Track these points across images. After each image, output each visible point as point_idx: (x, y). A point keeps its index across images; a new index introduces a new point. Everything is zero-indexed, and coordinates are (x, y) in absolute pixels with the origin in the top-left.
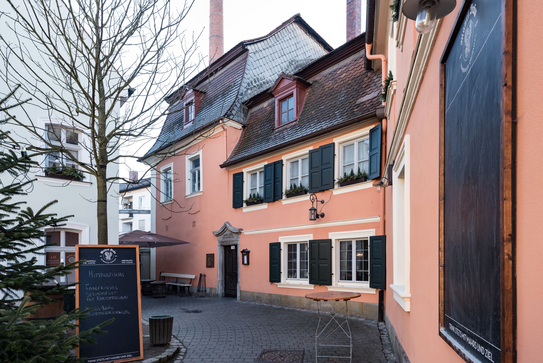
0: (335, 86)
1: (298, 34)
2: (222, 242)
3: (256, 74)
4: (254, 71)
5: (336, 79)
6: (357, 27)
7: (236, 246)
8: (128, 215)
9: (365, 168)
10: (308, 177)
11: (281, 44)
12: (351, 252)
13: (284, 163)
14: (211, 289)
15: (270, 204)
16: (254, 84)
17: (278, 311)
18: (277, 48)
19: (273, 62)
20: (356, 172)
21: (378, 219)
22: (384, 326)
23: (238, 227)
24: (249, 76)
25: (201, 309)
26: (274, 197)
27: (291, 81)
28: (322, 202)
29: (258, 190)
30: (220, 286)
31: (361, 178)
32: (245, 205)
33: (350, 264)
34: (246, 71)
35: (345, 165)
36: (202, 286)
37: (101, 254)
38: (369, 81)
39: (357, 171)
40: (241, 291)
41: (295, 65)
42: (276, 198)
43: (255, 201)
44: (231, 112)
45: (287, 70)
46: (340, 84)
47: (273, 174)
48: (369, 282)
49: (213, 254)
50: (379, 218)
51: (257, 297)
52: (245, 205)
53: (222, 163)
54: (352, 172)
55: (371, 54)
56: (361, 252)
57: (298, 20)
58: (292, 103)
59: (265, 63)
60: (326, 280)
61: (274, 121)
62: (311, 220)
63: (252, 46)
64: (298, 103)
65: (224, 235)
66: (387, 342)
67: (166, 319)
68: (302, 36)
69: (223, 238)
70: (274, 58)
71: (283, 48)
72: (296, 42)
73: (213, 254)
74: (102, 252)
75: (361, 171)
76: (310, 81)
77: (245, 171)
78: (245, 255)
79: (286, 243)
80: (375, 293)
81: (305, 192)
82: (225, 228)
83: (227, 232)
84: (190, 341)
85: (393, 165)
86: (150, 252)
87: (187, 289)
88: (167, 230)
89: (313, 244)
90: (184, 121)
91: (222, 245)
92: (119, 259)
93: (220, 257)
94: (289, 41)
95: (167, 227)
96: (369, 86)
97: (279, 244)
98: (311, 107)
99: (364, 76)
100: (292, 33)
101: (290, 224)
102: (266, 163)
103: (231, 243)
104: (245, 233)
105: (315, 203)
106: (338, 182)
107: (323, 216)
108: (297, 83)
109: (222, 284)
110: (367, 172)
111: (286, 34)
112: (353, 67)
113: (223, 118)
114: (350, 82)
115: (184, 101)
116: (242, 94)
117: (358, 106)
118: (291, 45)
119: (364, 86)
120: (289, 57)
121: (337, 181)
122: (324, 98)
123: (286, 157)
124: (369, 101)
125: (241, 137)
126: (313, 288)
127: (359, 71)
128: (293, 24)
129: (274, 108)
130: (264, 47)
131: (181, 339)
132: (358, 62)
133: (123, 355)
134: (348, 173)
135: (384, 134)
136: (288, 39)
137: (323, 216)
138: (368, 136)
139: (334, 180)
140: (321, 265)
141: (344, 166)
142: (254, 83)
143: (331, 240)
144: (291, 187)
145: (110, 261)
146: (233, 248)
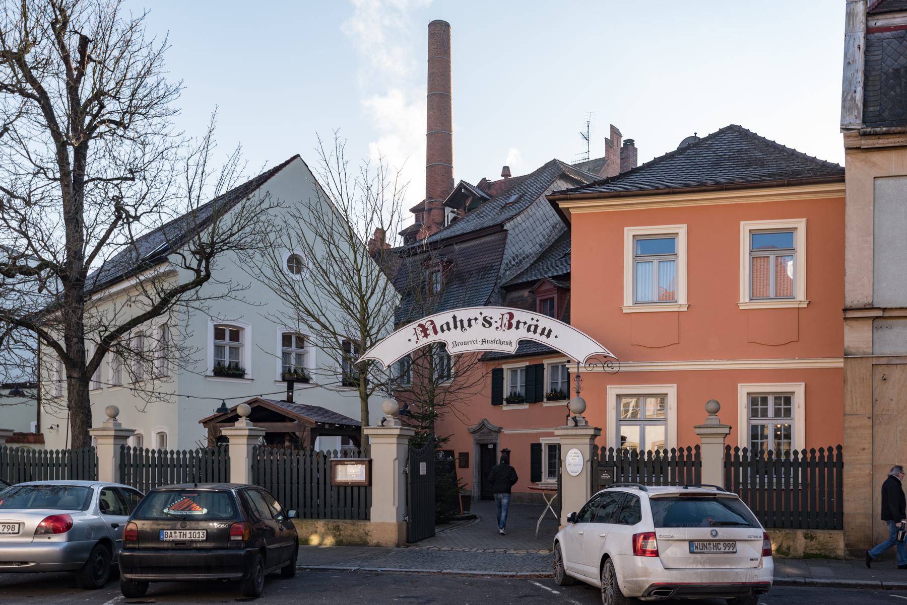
7: (495, 445)
13: (545, 366)
16: (513, 263)
23: (499, 426)
29: (519, 389)
32: (504, 402)
43: (514, 399)
52: (504, 402)
82: (483, 425)
83: (485, 430)
104: (506, 432)
146: (490, 446)
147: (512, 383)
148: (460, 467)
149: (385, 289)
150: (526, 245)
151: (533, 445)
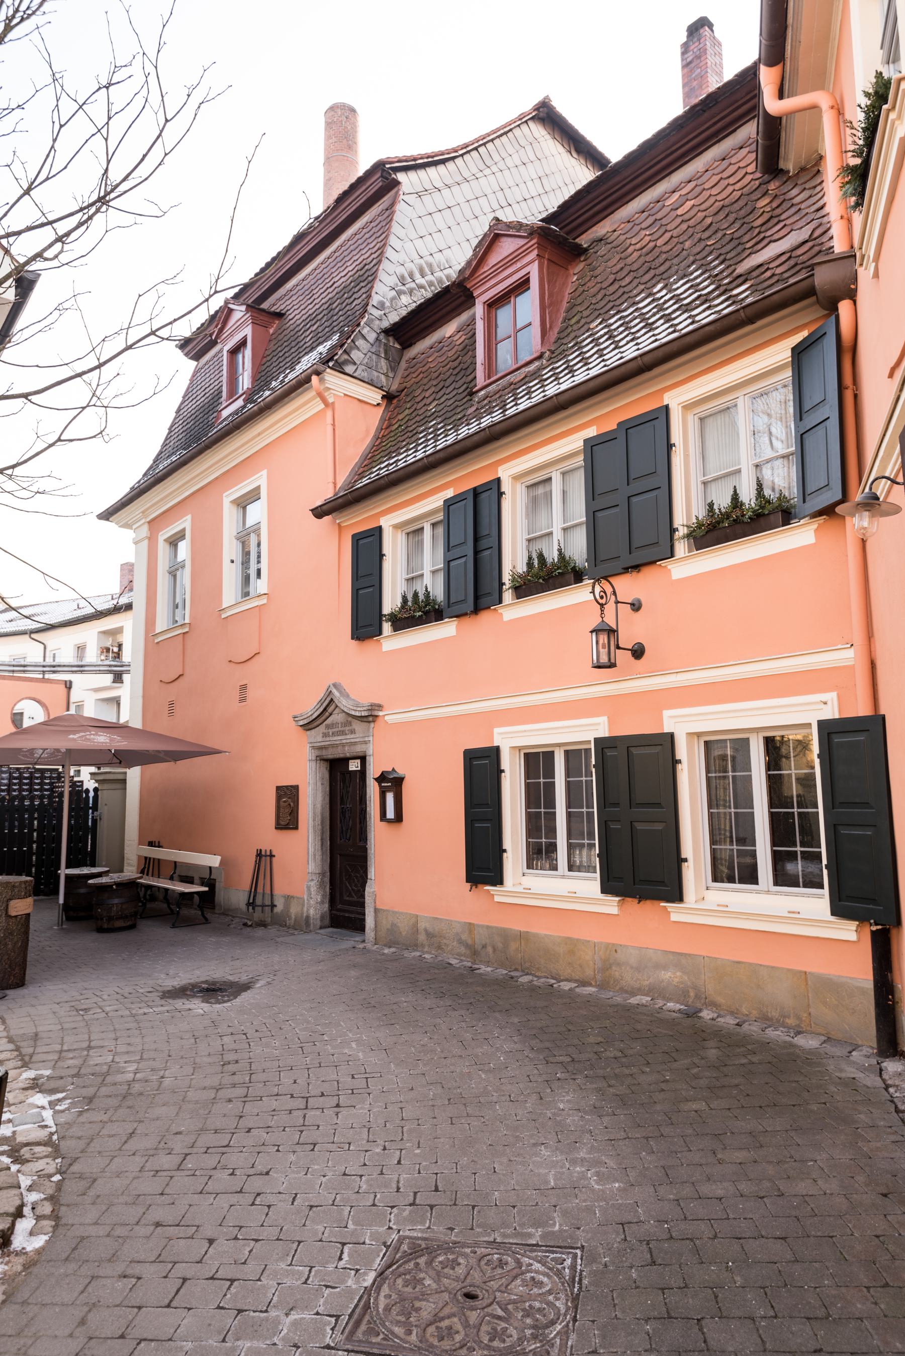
1: (547, 153)
2: (321, 748)
3: (424, 253)
4: (419, 243)
5: (664, 222)
7: (363, 759)
8: (110, 677)
10: (584, 528)
13: (506, 487)
14: (288, 899)
15: (467, 622)
16: (420, 281)
17: (496, 986)
18: (487, 184)
20: (748, 497)
21: (848, 656)
24: (401, 257)
26: (477, 597)
27: (521, 242)
28: (636, 606)
29: (427, 580)
30: (313, 889)
31: (770, 515)
32: (387, 627)
35: (709, 477)
36: (260, 890)
38: (774, 205)
39: (753, 493)
40: (376, 911)
42: (483, 601)
43: (419, 613)
46: (675, 233)
47: (475, 522)
48: (826, 891)
49: (296, 788)
50: (850, 654)
52: (387, 627)
53: (319, 503)
54: (735, 497)
55: (781, 96)
57: (546, 116)
58: (527, 307)
59: (451, 223)
60: (662, 883)
62: (599, 667)
63: (412, 175)
64: (546, 307)
65: (328, 727)
68: (558, 157)
69: (325, 735)
70: (478, 212)
72: (541, 174)
73: (296, 788)
75: (767, 492)
76: (584, 240)
77: (386, 522)
78: (388, 789)
79: (520, 749)
80: (853, 937)
81: (578, 576)
82: (328, 706)
83: (337, 717)
86: (124, 781)
88: (171, 713)
89: (609, 753)
90: (224, 394)
91: (321, 759)
93: (315, 796)
94: (522, 168)
95: (171, 704)
97: (494, 753)
98: (586, 313)
99: (758, 194)
101: (530, 685)
102: (450, 493)
103: (347, 752)
104: (389, 717)
105: (610, 608)
107: (638, 652)
108: (540, 246)
109: (321, 885)
111: (511, 150)
112: (715, 179)
113: (321, 367)
114: (708, 221)
118: (527, 179)
121: (682, 531)
122: (627, 280)
123: (511, 468)
124: (784, 258)
125: (380, 429)
126: (614, 910)
127: (738, 186)
130: (449, 181)
132: (733, 160)
134: (723, 502)
135: (848, 352)
136: (519, 163)
137: (638, 652)
138: (788, 373)
139: (673, 530)
140: (639, 826)
141: (705, 483)
142: (417, 275)
144: (530, 564)
146: (354, 766)
147: (409, 568)
148: (121, 870)
150: (456, 248)
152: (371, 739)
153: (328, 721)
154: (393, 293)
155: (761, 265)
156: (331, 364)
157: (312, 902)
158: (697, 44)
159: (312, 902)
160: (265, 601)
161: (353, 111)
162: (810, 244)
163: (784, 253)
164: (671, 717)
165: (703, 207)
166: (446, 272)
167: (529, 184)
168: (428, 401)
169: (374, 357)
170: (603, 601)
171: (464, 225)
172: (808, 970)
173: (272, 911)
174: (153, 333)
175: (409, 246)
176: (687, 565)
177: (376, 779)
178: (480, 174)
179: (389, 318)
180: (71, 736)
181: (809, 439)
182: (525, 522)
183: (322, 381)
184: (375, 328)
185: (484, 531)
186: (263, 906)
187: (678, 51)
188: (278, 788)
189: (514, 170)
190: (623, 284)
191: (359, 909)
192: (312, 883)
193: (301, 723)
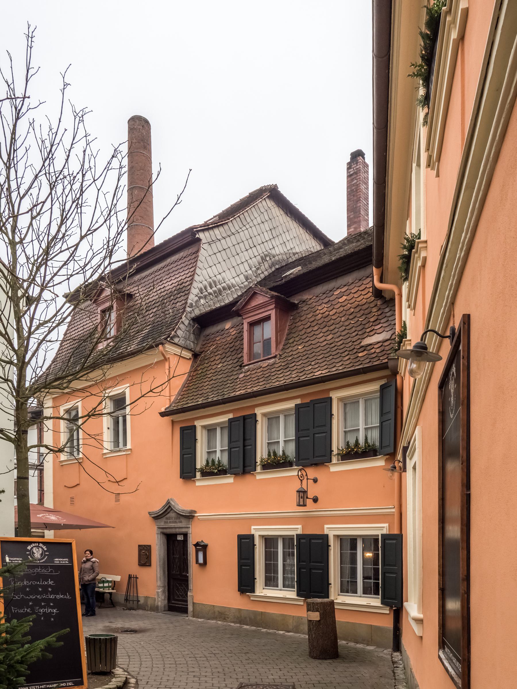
0: (331, 313)
1: (275, 215)
3: (212, 275)
4: (209, 270)
5: (333, 303)
6: (362, 212)
7: (186, 535)
9: (374, 436)
11: (250, 229)
12: (356, 554)
13: (259, 418)
14: (146, 598)
16: (210, 291)
19: (237, 257)
22: (400, 657)
23: (188, 508)
24: (201, 278)
25: (149, 626)
26: (244, 466)
29: (218, 454)
30: (160, 594)
31: (368, 452)
32: (198, 474)
33: (354, 571)
34: (198, 271)
37: (28, 551)
38: (379, 313)
41: (270, 262)
42: (247, 469)
43: (213, 471)
44: (175, 332)
45: (258, 269)
46: (338, 311)
47: (242, 432)
48: (380, 596)
49: (150, 546)
51: (219, 612)
52: (198, 474)
54: (357, 441)
56: (369, 551)
57: (273, 194)
58: (269, 330)
61: (242, 352)
63: (207, 233)
66: (402, 676)
67: (109, 639)
68: (280, 217)
70: (239, 251)
71: (252, 236)
72: (271, 227)
73: (150, 546)
74: (29, 548)
80: (388, 612)
82: (168, 508)
83: (172, 515)
84: (138, 669)
85: (408, 447)
87: (107, 596)
92: (51, 558)
94: (262, 225)
95: (72, 499)
96: (378, 321)
99: (372, 305)
100: (265, 213)
103: (178, 531)
105: (305, 482)
106: (338, 454)
108: (277, 303)
110: (377, 444)
111: (256, 215)
112: (356, 289)
113: (164, 341)
114: (352, 310)
115: (98, 305)
116: (191, 304)
117: (365, 348)
118: (264, 231)
119: (372, 320)
120: (261, 250)
121: (335, 452)
124: (380, 345)
127: (365, 297)
128: (267, 200)
129: (241, 332)
130: (224, 235)
131: (125, 667)
132: (365, 282)
133: (62, 683)
136: (260, 222)
142: (209, 288)
143: (327, 535)
144: (269, 455)
145: (39, 560)
146: (180, 538)
149: (130, 404)
150: (228, 272)
151: (241, 538)
152: (190, 526)
153: (168, 516)
154: (197, 298)
155: (371, 345)
156: (168, 339)
157: (160, 599)
158: (355, 165)
159: (160, 599)
160: (130, 453)
161: (147, 122)
162: (389, 342)
163: (380, 342)
164: (328, 528)
165: (351, 302)
166: (222, 285)
167: (265, 233)
168: (218, 362)
169: (188, 333)
170: (302, 479)
171: (232, 259)
172: (372, 624)
173: (138, 603)
174: (151, 391)
175: (204, 272)
176: (337, 467)
177: (194, 545)
178: (241, 230)
179: (195, 312)
180: (38, 516)
181: (384, 424)
182: (267, 434)
183: (164, 348)
184: (188, 317)
185: (247, 437)
186: (133, 601)
187: (345, 167)
188: (139, 546)
189: (257, 226)
190: (314, 330)
191: (185, 603)
192: (159, 591)
193: (153, 516)
